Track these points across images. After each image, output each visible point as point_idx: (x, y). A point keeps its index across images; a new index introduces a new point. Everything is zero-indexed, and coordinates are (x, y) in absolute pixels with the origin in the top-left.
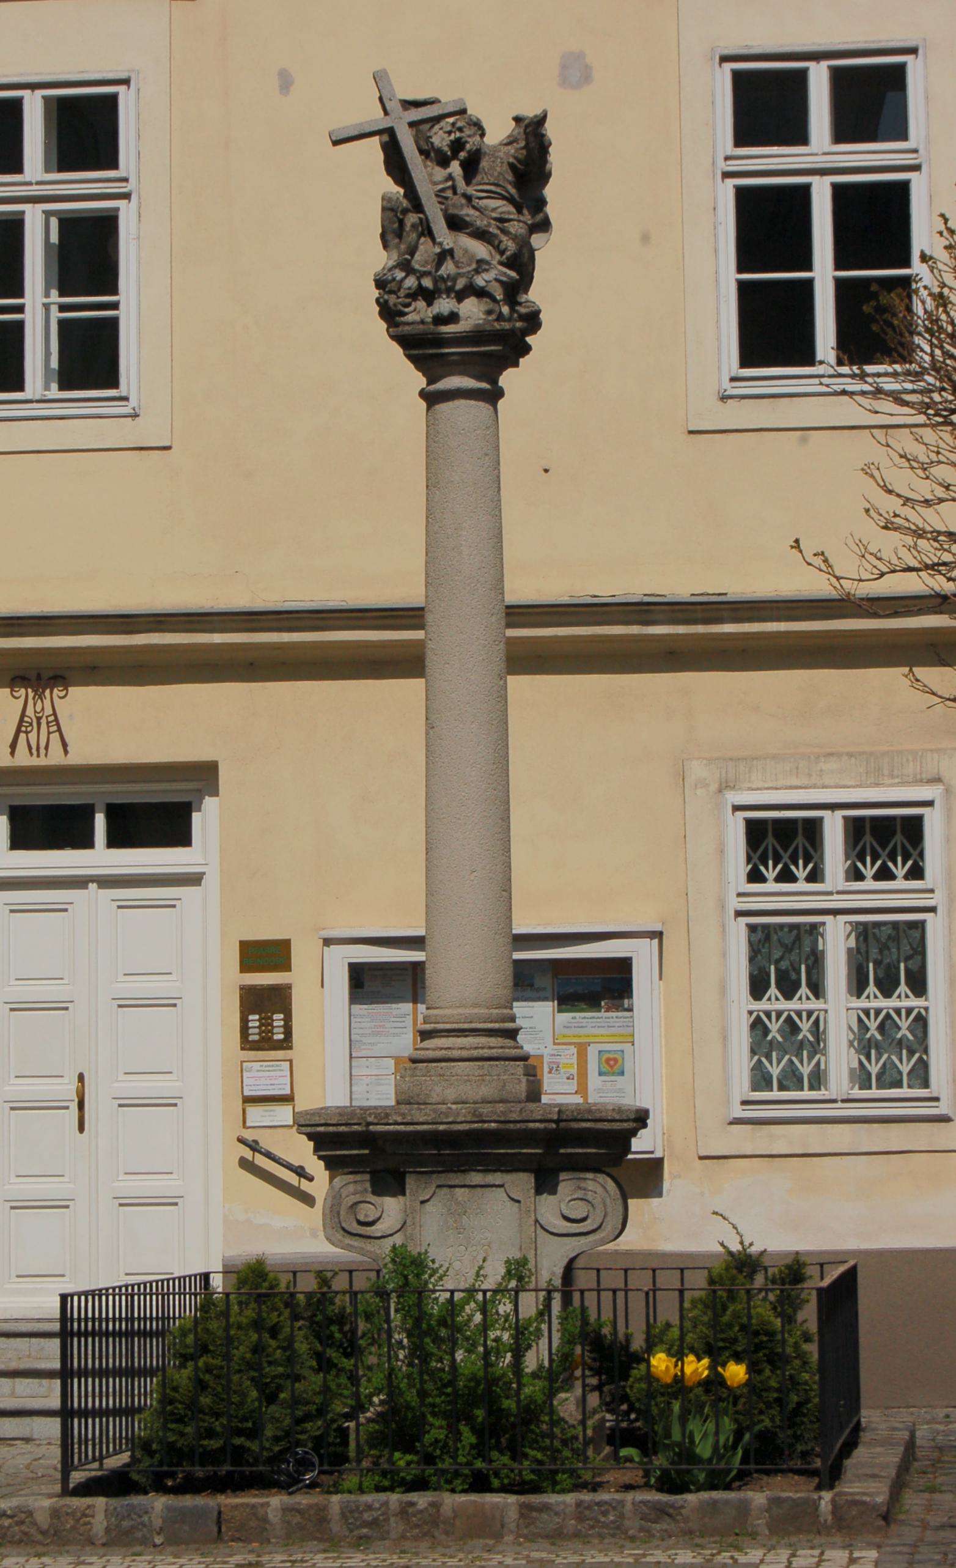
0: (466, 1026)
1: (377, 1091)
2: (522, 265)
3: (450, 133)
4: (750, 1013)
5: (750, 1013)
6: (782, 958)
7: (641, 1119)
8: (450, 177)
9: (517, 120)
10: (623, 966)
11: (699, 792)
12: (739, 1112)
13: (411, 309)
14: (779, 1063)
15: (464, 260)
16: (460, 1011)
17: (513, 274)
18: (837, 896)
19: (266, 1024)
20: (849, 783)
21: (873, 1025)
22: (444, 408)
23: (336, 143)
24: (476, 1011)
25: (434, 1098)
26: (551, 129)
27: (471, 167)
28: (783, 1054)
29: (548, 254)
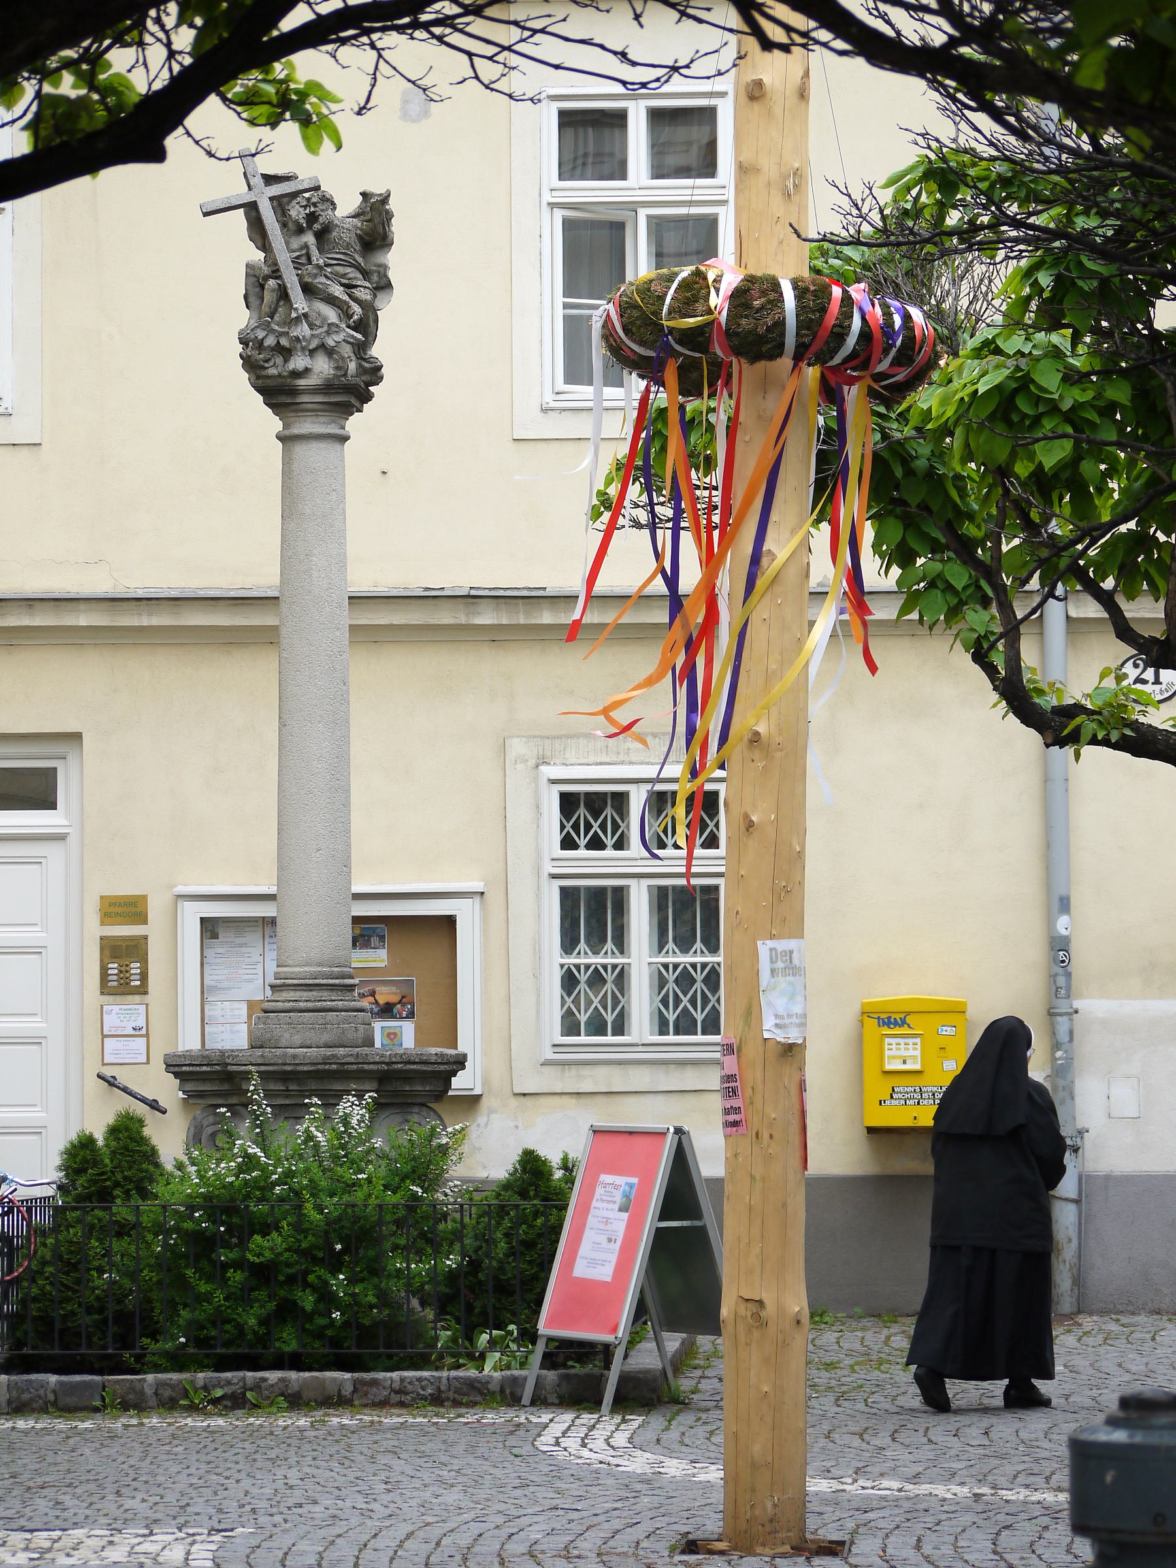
0: (311, 982)
1: (232, 1035)
2: (366, 326)
3: (305, 207)
4: (562, 966)
5: (562, 966)
6: (591, 914)
7: (460, 1062)
8: (306, 246)
9: (365, 195)
10: (449, 922)
11: (518, 766)
12: (550, 1055)
13: (271, 363)
14: (586, 1012)
15: (318, 323)
16: (306, 969)
17: (359, 336)
18: (635, 868)
19: (124, 972)
20: (652, 761)
21: (671, 977)
22: (300, 449)
23: (206, 214)
24: (320, 969)
25: (283, 1043)
26: (392, 205)
27: (322, 235)
28: (591, 1006)
29: (392, 317)
